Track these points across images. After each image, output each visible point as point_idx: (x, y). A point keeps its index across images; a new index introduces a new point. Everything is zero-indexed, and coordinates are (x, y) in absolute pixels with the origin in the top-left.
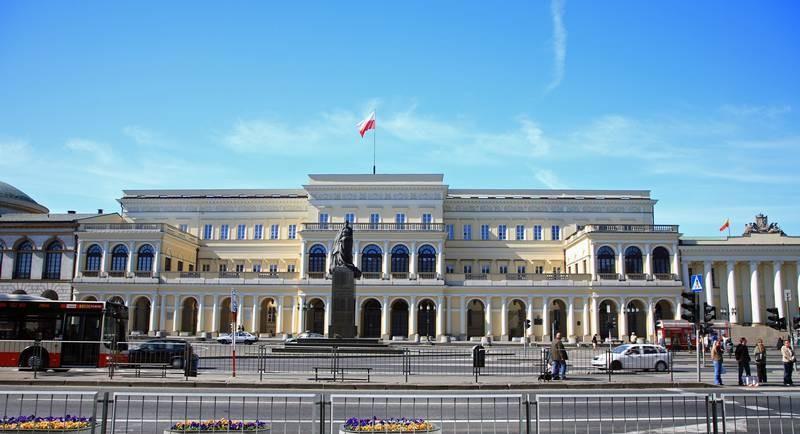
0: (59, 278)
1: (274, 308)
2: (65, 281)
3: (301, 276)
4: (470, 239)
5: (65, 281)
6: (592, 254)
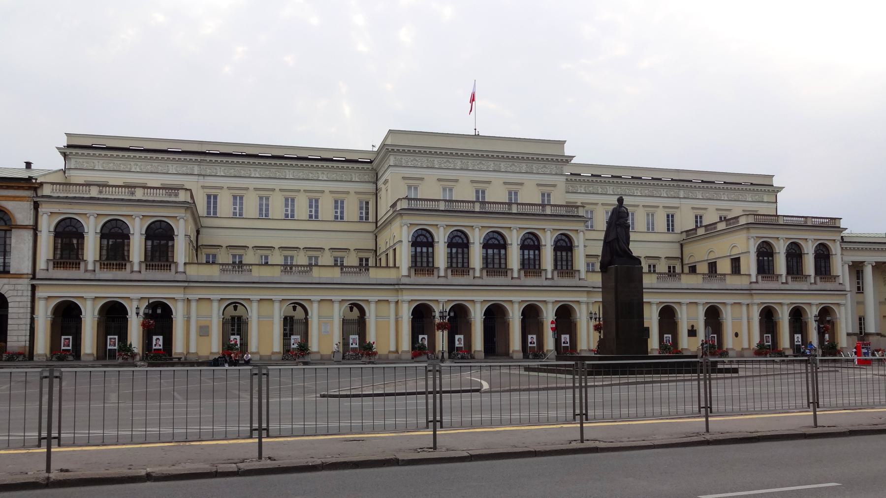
1: (239, 318)
2: (19, 276)
3: (404, 272)
4: (267, 217)
5: (19, 276)
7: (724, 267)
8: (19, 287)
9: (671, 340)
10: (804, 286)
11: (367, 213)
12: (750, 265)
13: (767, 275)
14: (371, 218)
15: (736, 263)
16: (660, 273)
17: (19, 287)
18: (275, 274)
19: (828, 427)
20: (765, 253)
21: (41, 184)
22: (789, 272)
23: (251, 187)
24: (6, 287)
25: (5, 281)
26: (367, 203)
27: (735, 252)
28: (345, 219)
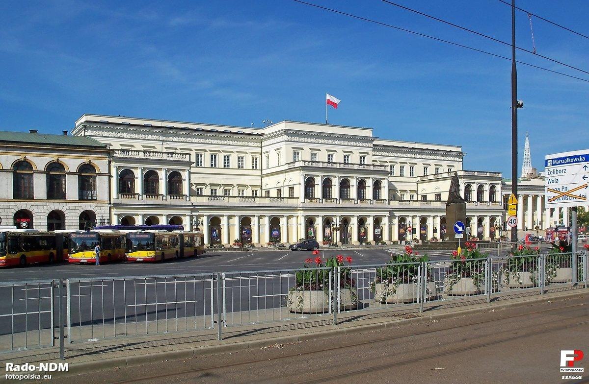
0: (33, 198)
2: (103, 202)
5: (103, 202)
6: (302, 182)
7: (286, 193)
8: (103, 208)
9: (388, 251)
10: (159, 201)
11: (256, 164)
12: (299, 191)
13: (126, 193)
14: (259, 167)
15: (438, 196)
16: (272, 197)
17: (103, 208)
18: (236, 202)
19: (312, 313)
20: (309, 183)
21: (113, 150)
22: (341, 197)
23: (221, 150)
24: (96, 208)
25: (96, 204)
26: (256, 159)
27: (438, 191)
28: (244, 168)
